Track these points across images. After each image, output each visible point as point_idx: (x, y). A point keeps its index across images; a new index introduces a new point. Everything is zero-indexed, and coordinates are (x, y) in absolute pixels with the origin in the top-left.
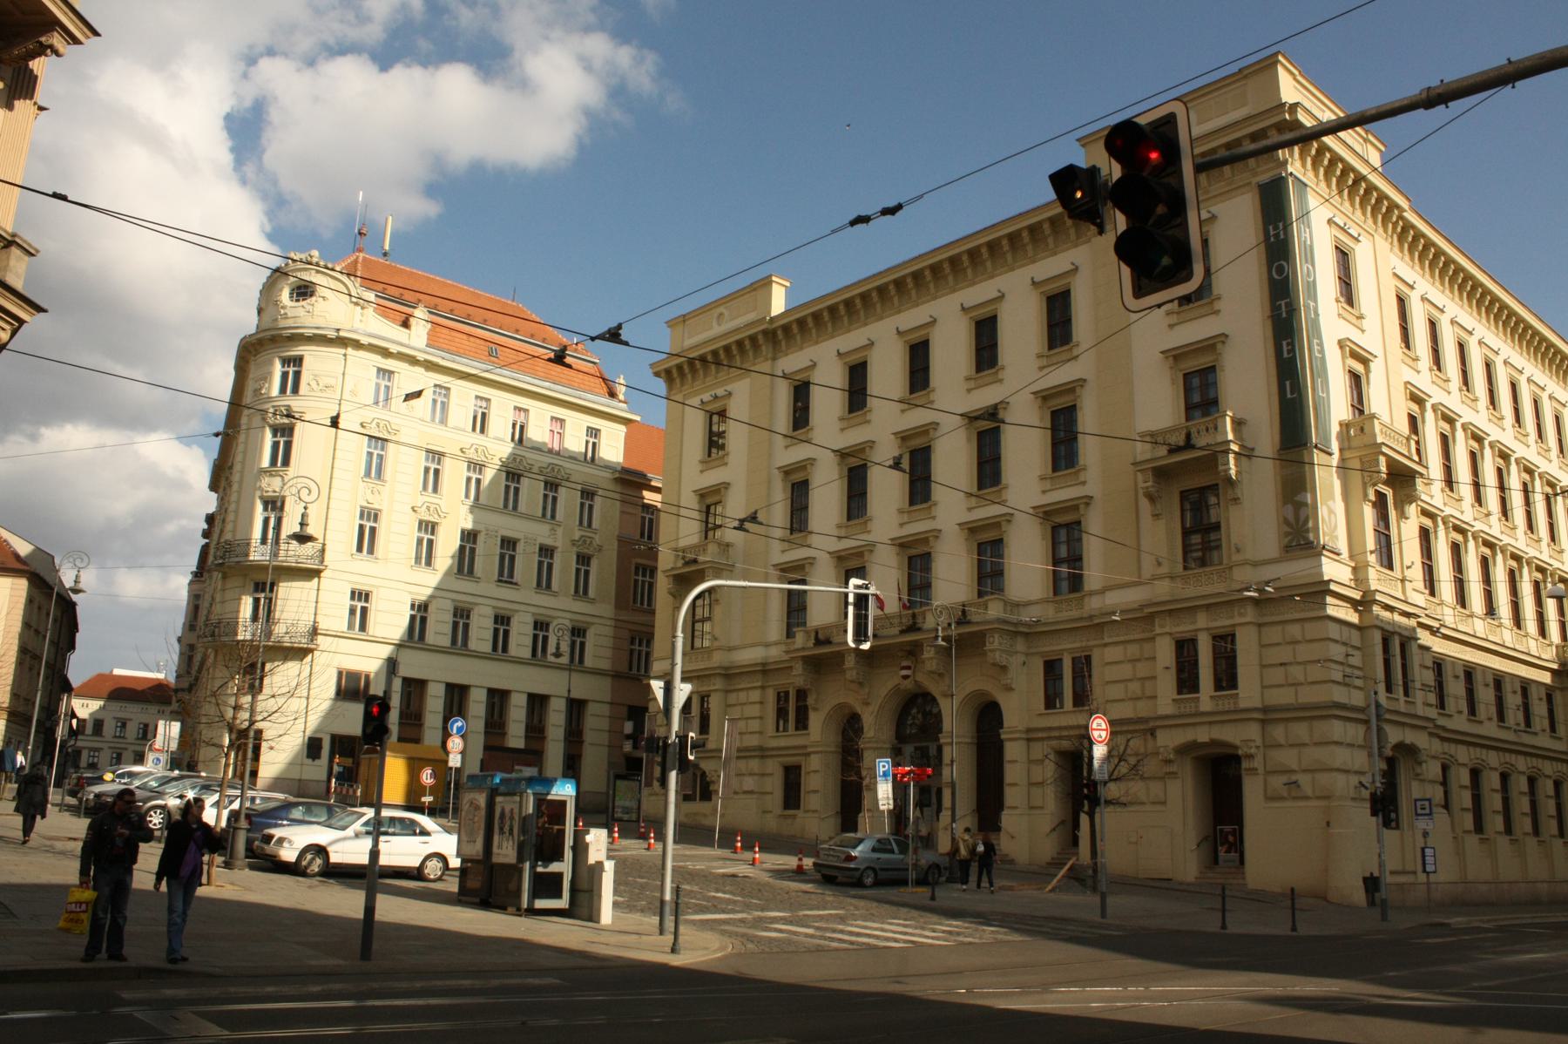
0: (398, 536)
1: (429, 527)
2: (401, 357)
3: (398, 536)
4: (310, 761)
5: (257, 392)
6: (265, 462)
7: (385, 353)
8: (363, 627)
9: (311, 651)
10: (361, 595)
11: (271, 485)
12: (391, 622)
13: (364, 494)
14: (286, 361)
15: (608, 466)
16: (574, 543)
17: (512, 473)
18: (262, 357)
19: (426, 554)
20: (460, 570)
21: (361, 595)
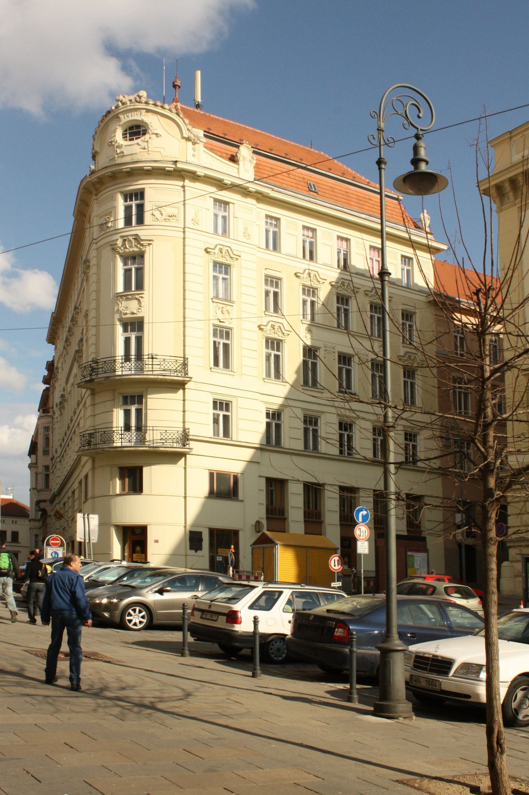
0: (249, 350)
1: (274, 344)
2: (234, 188)
3: (249, 350)
4: (193, 552)
5: (103, 226)
6: (120, 288)
7: (220, 185)
8: (226, 434)
9: (183, 455)
10: (222, 405)
11: (130, 308)
12: (251, 427)
13: (214, 313)
14: (128, 196)
15: (421, 291)
17: (342, 298)
18: (105, 194)
19: (275, 368)
20: (306, 383)
21: (222, 405)
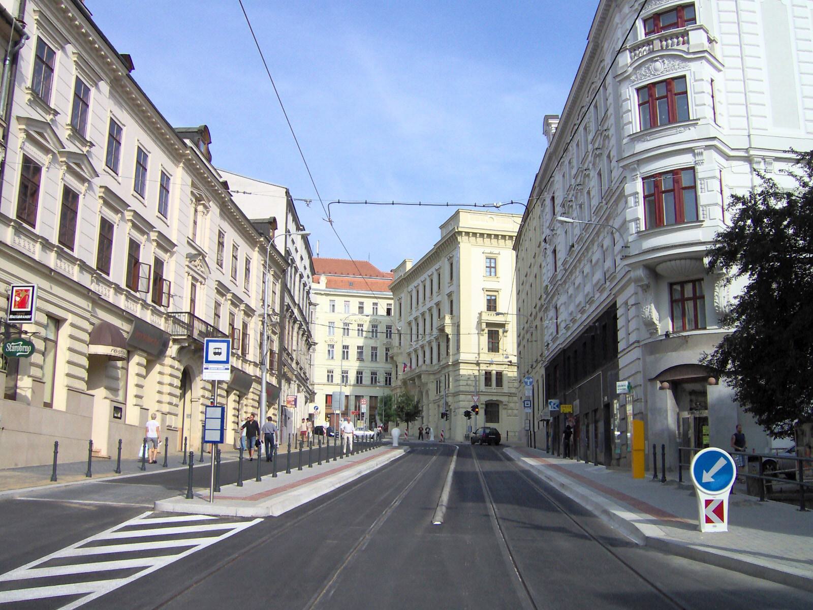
16: (384, 344)
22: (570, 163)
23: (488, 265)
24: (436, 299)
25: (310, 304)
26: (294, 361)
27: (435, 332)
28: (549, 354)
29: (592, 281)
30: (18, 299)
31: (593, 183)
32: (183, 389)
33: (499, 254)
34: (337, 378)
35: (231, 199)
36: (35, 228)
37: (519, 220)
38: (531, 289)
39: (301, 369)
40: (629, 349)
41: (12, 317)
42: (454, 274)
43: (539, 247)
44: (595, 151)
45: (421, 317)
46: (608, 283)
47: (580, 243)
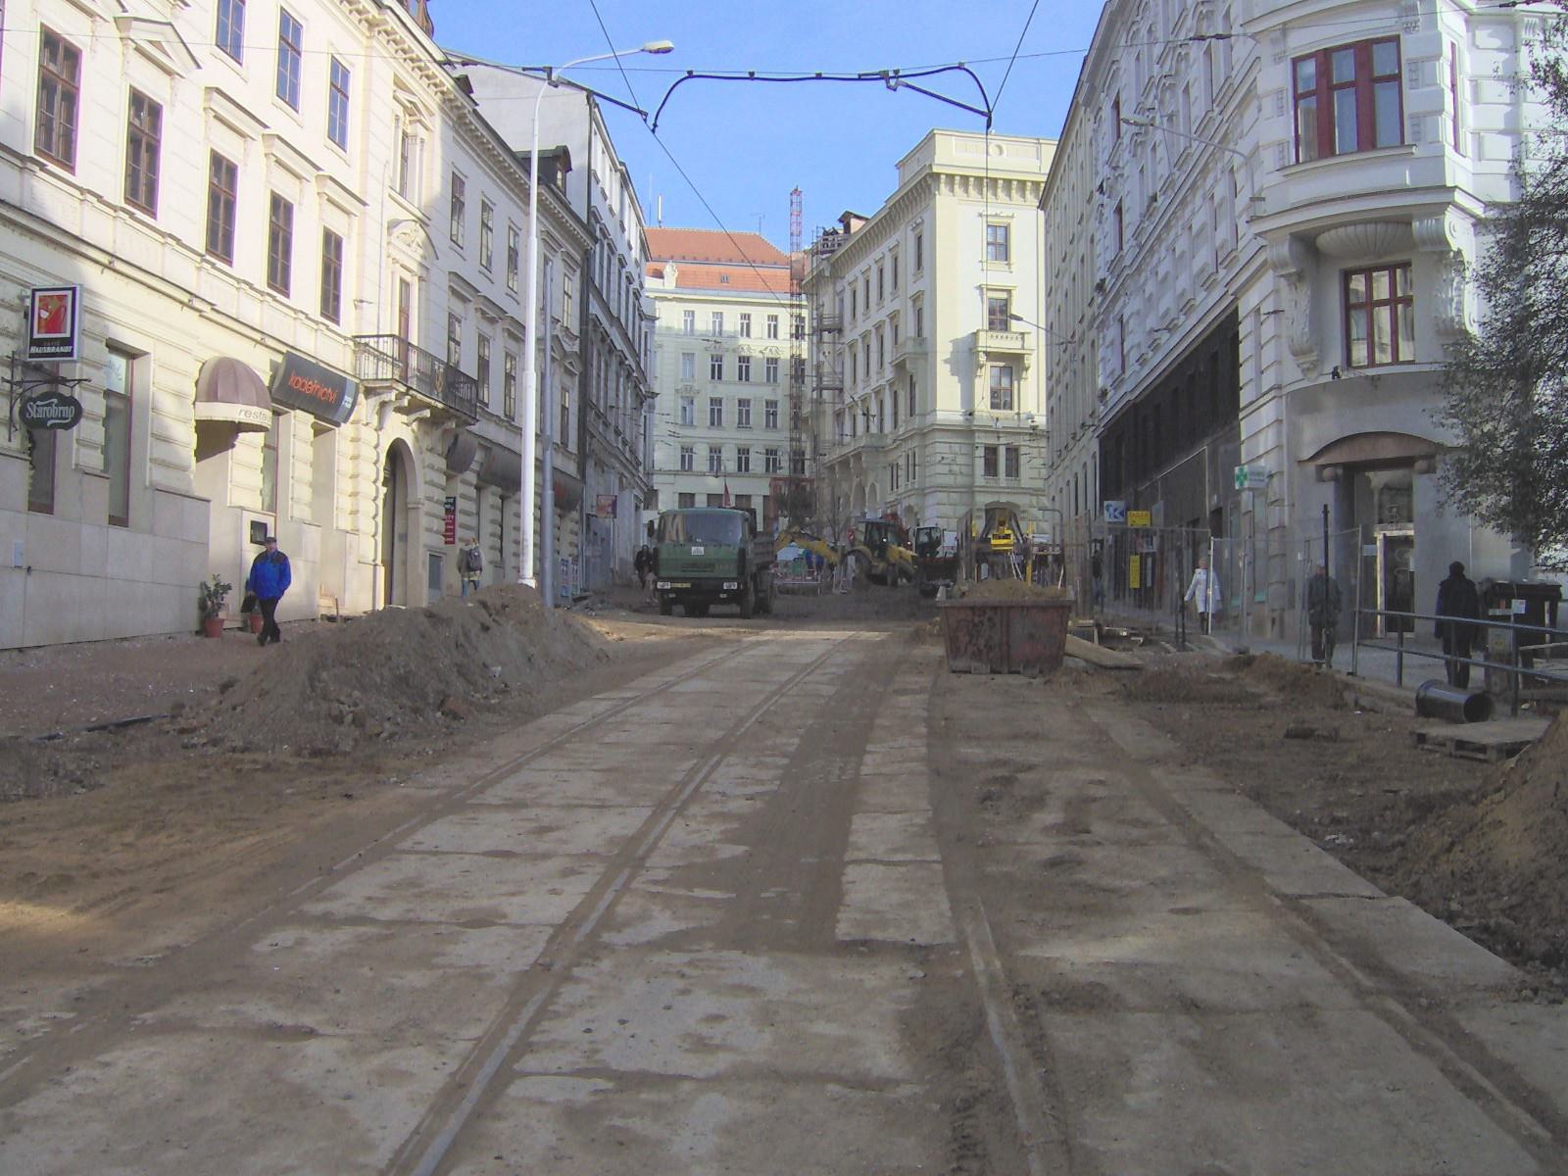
22: (1150, 31)
23: (990, 240)
24: (890, 306)
25: (642, 317)
26: (612, 429)
27: (889, 373)
28: (1106, 412)
29: (1213, 238)
30: (45, 315)
31: (1195, 72)
32: (390, 485)
33: (1012, 217)
34: (701, 462)
35: (475, 111)
36: (155, 218)
37: (1049, 151)
38: (1082, 269)
39: (625, 443)
40: (1262, 401)
41: (34, 350)
42: (922, 257)
43: (1089, 201)
44: (1164, 81)
45: (860, 340)
46: (1222, 272)
47: (1169, 192)
